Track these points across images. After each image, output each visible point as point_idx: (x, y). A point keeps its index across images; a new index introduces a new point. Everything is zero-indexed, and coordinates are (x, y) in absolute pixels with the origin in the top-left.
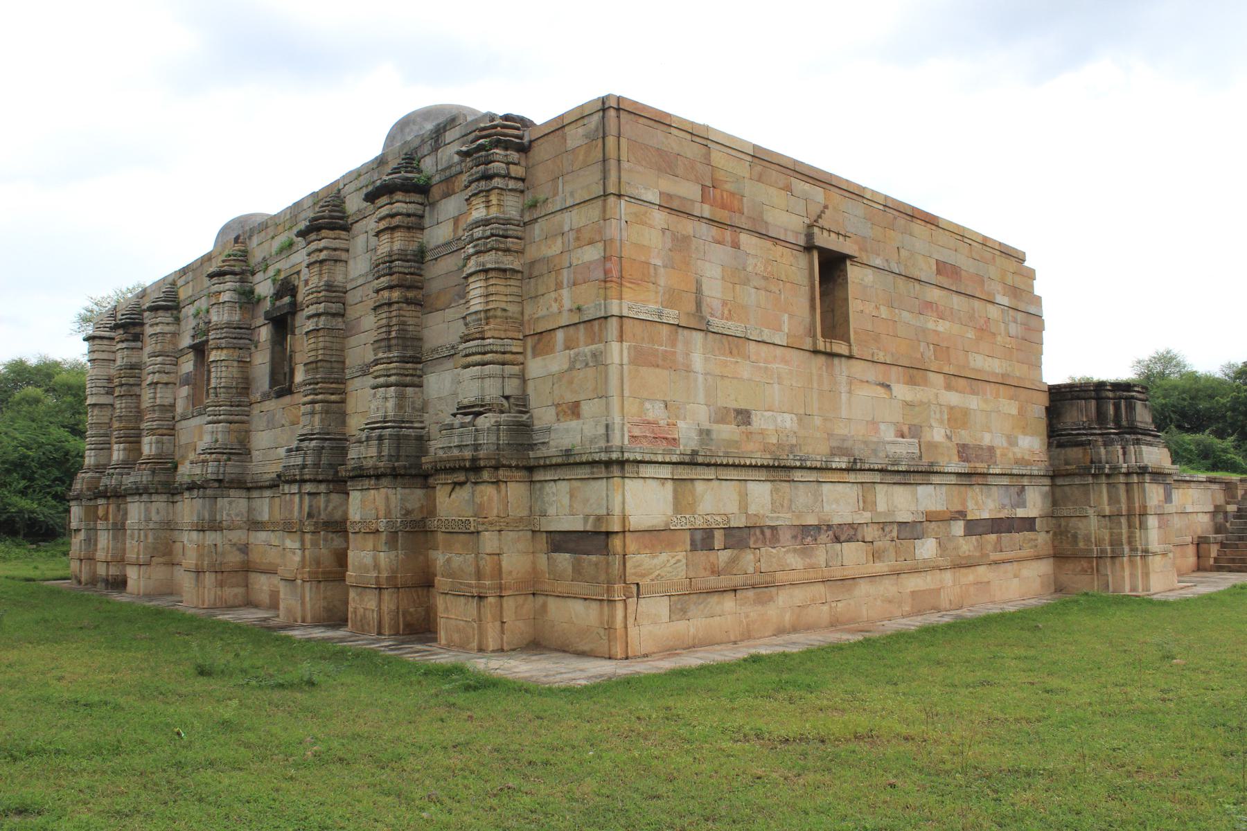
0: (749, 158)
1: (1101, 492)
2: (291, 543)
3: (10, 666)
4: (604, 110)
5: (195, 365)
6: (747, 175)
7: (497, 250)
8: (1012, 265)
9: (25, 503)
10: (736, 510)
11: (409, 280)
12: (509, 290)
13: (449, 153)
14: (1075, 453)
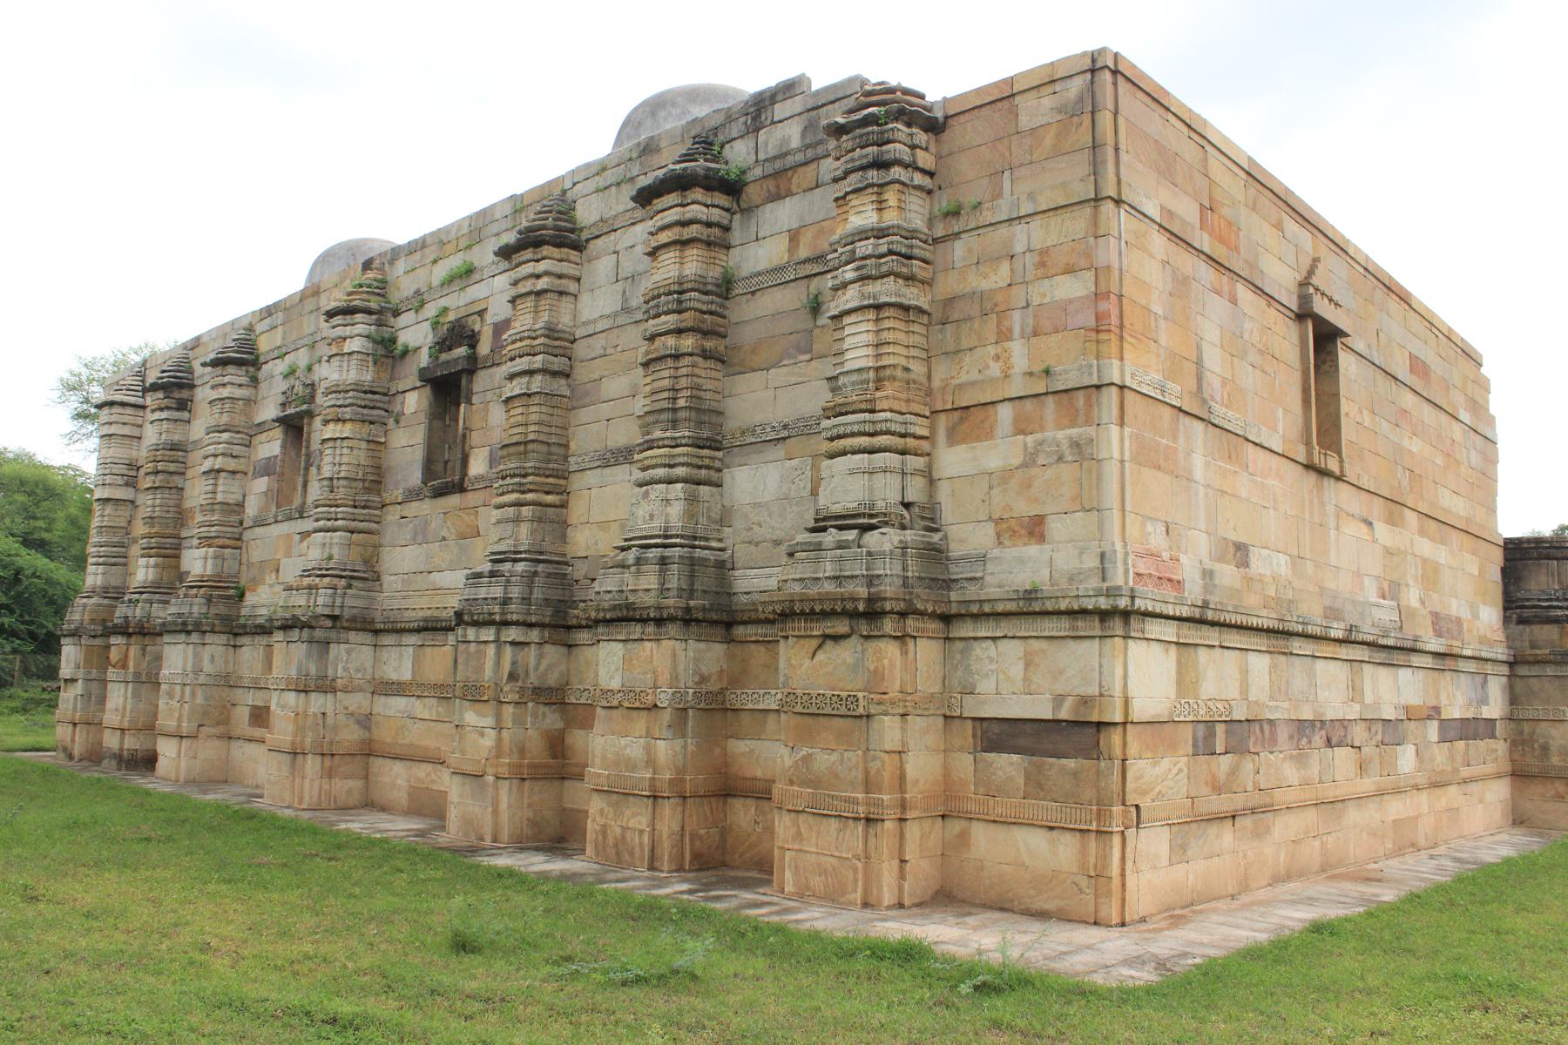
0: (1243, 175)
5: (283, 447)
7: (897, 275)
10: (1237, 696)
11: (705, 324)
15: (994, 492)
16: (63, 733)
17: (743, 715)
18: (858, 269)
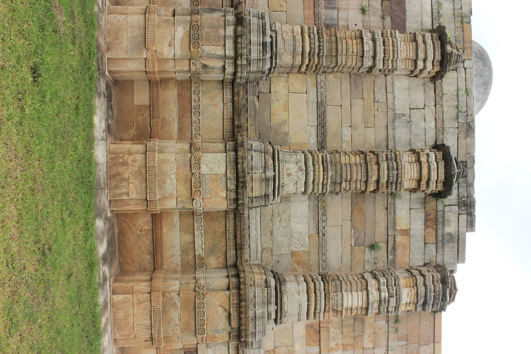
15: (286, 348)
17: (191, 219)
18: (385, 299)
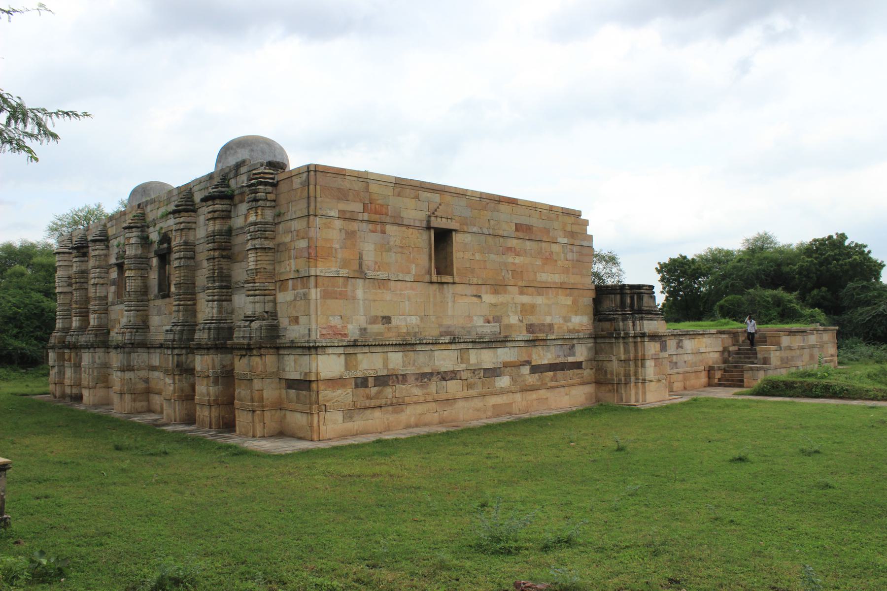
1: (619, 347)
2: (168, 380)
3: (27, 446)
4: (309, 171)
6: (391, 194)
8: (571, 219)
9: (17, 343)
10: (381, 367)
11: (224, 246)
12: (267, 258)
13: (243, 180)
14: (607, 325)
16: (51, 388)
